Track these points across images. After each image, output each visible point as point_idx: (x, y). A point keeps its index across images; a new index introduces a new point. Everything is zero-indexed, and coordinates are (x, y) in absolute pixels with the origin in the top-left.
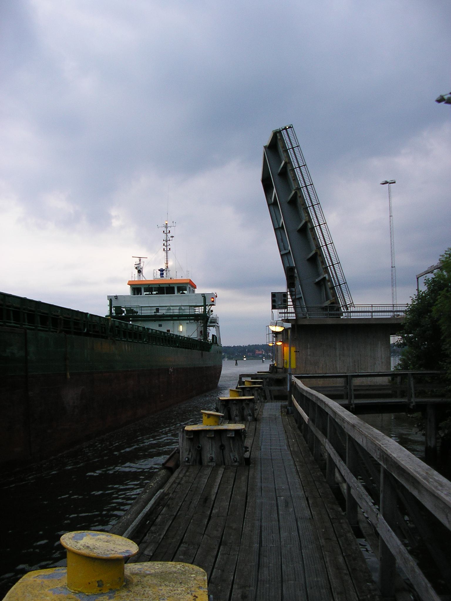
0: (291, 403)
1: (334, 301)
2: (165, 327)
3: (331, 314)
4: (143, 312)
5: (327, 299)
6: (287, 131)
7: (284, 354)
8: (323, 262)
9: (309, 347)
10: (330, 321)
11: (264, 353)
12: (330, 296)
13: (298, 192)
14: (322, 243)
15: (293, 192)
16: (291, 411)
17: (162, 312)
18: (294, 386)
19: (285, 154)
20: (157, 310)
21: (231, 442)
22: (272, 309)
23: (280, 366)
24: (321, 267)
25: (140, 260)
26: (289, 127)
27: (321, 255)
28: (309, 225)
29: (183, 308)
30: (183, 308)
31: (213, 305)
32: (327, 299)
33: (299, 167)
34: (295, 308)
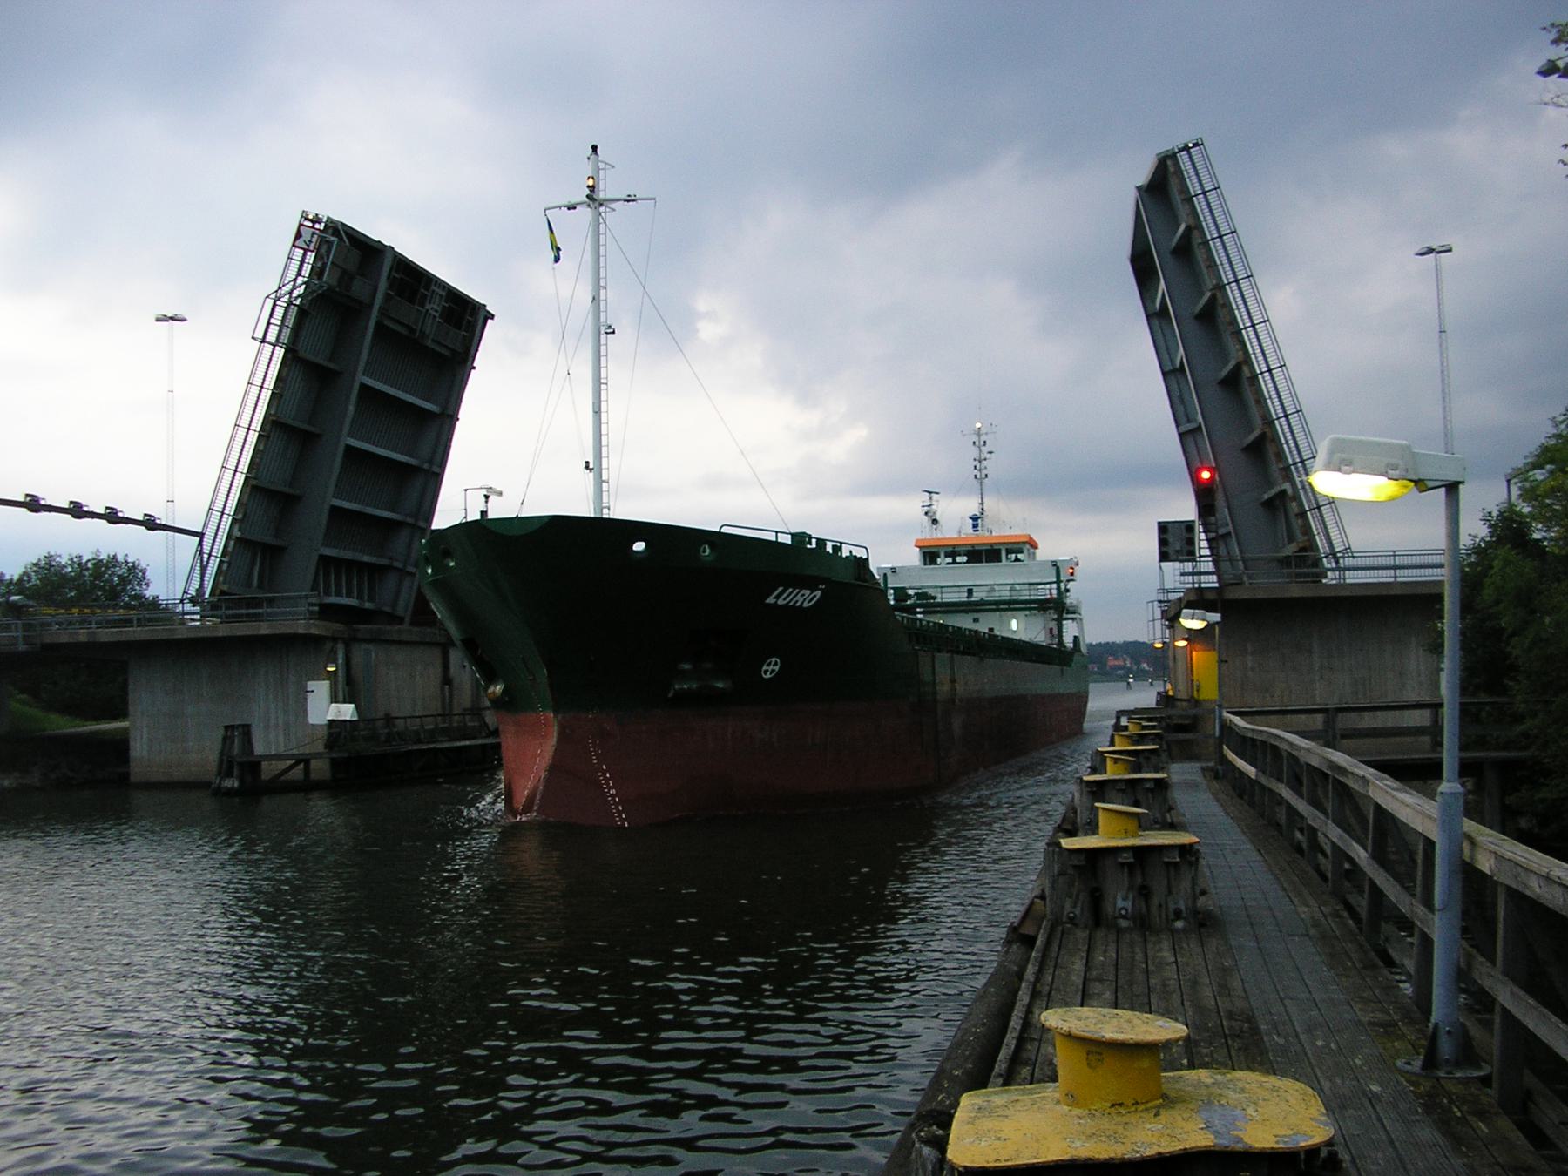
0: (1223, 760)
1: (1307, 544)
2: (985, 624)
3: (1298, 575)
4: (944, 596)
5: (1291, 539)
6: (1189, 153)
7: (1192, 666)
8: (1280, 455)
9: (1250, 649)
10: (1296, 591)
11: (1129, 665)
12: (1298, 532)
13: (1219, 296)
14: (1275, 410)
15: (1208, 294)
16: (1223, 774)
17: (977, 596)
18: (1226, 728)
19: (1187, 207)
20: (970, 592)
21: (1150, 796)
22: (1161, 561)
23: (1183, 695)
24: (1275, 467)
25: (931, 498)
26: (1195, 145)
27: (1276, 439)
28: (1246, 372)
29: (1018, 587)
30: (1018, 587)
31: (1072, 580)
32: (1291, 539)
33: (1221, 237)
34: (1215, 562)
